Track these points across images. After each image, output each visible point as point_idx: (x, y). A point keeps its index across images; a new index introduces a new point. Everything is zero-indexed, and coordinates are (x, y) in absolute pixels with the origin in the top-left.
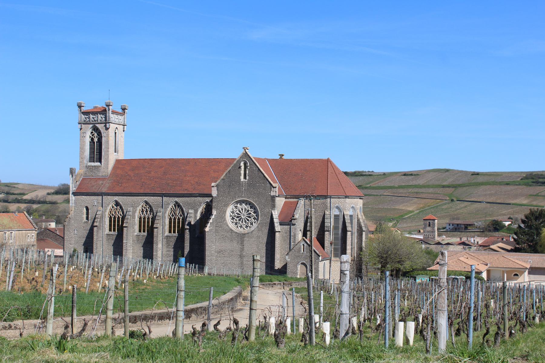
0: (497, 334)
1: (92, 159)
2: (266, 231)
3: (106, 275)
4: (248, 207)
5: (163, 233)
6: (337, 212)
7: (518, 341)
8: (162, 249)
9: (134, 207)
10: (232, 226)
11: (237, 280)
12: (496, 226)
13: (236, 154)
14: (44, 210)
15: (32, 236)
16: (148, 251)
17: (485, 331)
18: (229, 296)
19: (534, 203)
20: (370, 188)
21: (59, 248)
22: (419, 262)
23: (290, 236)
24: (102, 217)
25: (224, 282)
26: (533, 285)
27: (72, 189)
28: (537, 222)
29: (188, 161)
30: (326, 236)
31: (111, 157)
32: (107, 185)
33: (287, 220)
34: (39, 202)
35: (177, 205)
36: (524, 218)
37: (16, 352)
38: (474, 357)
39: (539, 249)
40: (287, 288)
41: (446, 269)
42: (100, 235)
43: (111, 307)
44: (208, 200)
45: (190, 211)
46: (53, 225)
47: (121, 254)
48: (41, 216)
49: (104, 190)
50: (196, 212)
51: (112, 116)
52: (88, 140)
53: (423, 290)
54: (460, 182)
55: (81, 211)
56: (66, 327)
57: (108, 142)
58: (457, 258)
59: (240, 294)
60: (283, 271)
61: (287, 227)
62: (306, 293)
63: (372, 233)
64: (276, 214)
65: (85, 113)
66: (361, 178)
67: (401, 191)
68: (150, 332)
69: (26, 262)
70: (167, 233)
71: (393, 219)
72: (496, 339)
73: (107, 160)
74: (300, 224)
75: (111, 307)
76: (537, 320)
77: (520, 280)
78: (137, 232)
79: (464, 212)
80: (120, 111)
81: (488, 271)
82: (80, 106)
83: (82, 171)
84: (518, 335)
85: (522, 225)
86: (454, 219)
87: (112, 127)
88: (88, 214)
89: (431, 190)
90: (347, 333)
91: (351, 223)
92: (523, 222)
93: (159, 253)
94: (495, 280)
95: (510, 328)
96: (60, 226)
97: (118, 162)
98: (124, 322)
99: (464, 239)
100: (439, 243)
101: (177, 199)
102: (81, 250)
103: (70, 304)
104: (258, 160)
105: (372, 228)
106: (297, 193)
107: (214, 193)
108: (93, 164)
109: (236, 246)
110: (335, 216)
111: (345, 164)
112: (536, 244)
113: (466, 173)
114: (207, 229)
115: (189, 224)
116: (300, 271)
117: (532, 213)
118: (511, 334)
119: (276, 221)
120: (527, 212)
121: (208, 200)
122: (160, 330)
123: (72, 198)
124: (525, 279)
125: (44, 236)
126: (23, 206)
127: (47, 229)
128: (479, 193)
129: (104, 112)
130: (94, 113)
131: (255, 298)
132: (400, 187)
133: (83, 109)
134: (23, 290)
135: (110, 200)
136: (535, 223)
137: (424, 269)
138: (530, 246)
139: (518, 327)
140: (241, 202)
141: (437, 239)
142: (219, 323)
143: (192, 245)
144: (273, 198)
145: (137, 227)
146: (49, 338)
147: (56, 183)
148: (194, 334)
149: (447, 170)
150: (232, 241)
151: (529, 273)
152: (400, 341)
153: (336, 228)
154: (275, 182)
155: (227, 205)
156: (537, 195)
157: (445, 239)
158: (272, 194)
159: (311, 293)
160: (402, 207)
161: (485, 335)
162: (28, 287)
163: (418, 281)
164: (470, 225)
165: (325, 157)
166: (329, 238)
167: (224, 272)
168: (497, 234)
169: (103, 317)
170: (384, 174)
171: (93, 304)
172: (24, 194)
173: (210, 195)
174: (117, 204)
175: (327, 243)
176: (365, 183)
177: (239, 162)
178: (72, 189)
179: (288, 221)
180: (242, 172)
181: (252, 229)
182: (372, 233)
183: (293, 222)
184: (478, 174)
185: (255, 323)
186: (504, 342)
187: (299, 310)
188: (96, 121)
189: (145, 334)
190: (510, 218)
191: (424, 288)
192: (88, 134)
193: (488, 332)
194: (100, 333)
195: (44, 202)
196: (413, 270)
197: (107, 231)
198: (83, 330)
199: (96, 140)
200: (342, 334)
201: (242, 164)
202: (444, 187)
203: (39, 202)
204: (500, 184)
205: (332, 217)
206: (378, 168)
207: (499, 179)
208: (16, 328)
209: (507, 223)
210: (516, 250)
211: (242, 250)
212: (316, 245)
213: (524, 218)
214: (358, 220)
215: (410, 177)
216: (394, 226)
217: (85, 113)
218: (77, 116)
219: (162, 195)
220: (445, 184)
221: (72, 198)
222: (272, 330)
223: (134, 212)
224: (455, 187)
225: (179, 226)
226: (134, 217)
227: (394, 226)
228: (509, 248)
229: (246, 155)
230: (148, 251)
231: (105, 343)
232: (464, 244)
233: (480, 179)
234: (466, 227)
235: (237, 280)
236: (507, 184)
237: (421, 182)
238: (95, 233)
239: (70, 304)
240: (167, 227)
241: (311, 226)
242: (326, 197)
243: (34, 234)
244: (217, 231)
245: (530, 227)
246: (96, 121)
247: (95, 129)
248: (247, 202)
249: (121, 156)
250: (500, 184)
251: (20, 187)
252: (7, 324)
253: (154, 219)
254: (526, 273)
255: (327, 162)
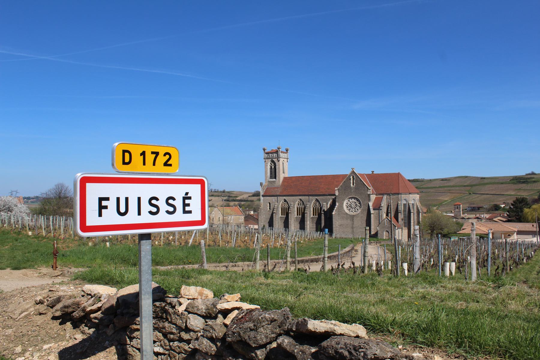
0: (503, 269)
1: (271, 177)
2: (366, 213)
3: (276, 237)
4: (355, 201)
5: (310, 216)
6: (405, 203)
7: (516, 273)
8: (309, 225)
9: (294, 202)
10: (347, 211)
11: (351, 241)
12: (496, 208)
13: (348, 172)
14: (247, 204)
15: (242, 219)
16: (302, 226)
17: (496, 268)
18: (347, 249)
19: (518, 194)
20: (423, 188)
21: (256, 225)
22: (452, 230)
23: (379, 216)
24: (278, 207)
25: (345, 242)
26: (520, 240)
27: (262, 193)
28: (521, 205)
29: (322, 177)
30: (400, 216)
31: (281, 176)
32: (280, 191)
33: (377, 207)
34: (245, 201)
35: (317, 200)
36: (512, 203)
37: (244, 279)
38: (495, 282)
39: (522, 220)
40: (378, 245)
41: (475, 232)
42: (277, 217)
43: (289, 255)
44: (333, 197)
45: (324, 204)
46: (252, 213)
47: (288, 228)
48: (246, 208)
49: (278, 194)
50: (327, 204)
51: (281, 154)
52: (269, 167)
53: (456, 244)
54: (474, 183)
55: (267, 205)
56: (265, 266)
57: (279, 168)
58: (476, 226)
59: (353, 248)
60: (376, 235)
61: (377, 211)
62: (394, 248)
63: (425, 213)
64: (371, 204)
65: (267, 153)
66: (417, 183)
67: (440, 189)
68: (309, 269)
69: (241, 232)
70: (312, 216)
71: (436, 205)
72: (502, 271)
73: (279, 177)
74: (384, 210)
75: (289, 255)
76: (525, 261)
77: (512, 238)
78: (296, 216)
79: (477, 200)
80: (285, 151)
81: (493, 233)
82: (264, 150)
83: (266, 184)
84: (514, 270)
85: (512, 207)
86: (471, 204)
87: (281, 160)
88: (270, 206)
89: (457, 188)
90: (419, 269)
91: (413, 208)
92: (512, 205)
93: (308, 227)
94: (497, 239)
95: (510, 266)
96: (256, 213)
97: (285, 178)
98: (295, 263)
99: (478, 215)
100: (463, 218)
101: (316, 197)
102: (267, 226)
103: (266, 254)
104: (360, 175)
105: (425, 211)
106: (382, 192)
107: (337, 193)
108: (272, 180)
109: (349, 222)
110: (404, 204)
111: (408, 175)
112: (521, 217)
113: (477, 178)
114: (333, 213)
115: (324, 210)
116: (385, 235)
117: (517, 200)
118: (510, 269)
119: (371, 208)
120: (515, 199)
121: (333, 197)
122: (315, 268)
123: (262, 198)
124: (515, 237)
125: (248, 219)
126: (237, 203)
127: (249, 215)
128: (486, 189)
129: (277, 152)
130: (271, 153)
131: (367, 251)
132: (440, 187)
133: (266, 151)
134: (240, 247)
135: (281, 199)
136: (519, 205)
137: (455, 233)
138: (517, 219)
139: (514, 265)
140: (351, 198)
141: (462, 215)
142: (344, 264)
143: (325, 221)
144: (369, 195)
145: (296, 213)
146: (259, 272)
147: (253, 190)
148: (332, 270)
149: (467, 177)
150: (347, 219)
151: (517, 234)
152: (447, 273)
153: (404, 211)
154: (370, 187)
155: (344, 200)
156: (520, 189)
157: (466, 216)
158: (369, 193)
159: (393, 247)
160: (440, 198)
161: (497, 269)
162: (242, 245)
163: (452, 239)
164: (481, 207)
165: (397, 172)
166: (401, 216)
167: (343, 236)
168: (497, 212)
169: (285, 260)
170: (430, 180)
171: (278, 254)
172: (237, 197)
173: (334, 195)
174: (285, 201)
175: (400, 220)
176: (420, 185)
177: (350, 176)
178: (262, 193)
179: (378, 207)
180: (352, 182)
181: (358, 212)
182: (425, 213)
183: (381, 208)
184: (484, 178)
185: (367, 264)
186: (507, 273)
187: (389, 256)
188: (273, 157)
189: (306, 270)
190: (504, 203)
191: (456, 243)
192: (269, 164)
193: (498, 268)
194: (282, 269)
195: (247, 201)
196: (449, 233)
197: (280, 215)
198: (274, 267)
199: (273, 167)
200: (416, 269)
201: (351, 177)
202: (465, 186)
203: (245, 201)
204: (498, 183)
205: (402, 205)
206: (427, 177)
207: (497, 181)
208: (238, 266)
209: (502, 206)
210: (508, 221)
211: (353, 224)
212: (394, 221)
213: (512, 203)
214: (417, 206)
215: (445, 181)
216: (437, 209)
217: (267, 153)
218: (262, 155)
219: (309, 195)
220: (465, 184)
221: (262, 198)
222: (374, 268)
223: (294, 205)
224: (472, 186)
225: (318, 212)
226: (294, 208)
227: (437, 209)
228: (504, 220)
229: (353, 172)
230: (302, 226)
231: (288, 275)
232: (477, 218)
233: (486, 181)
234: (479, 208)
235: (351, 241)
236: (502, 183)
237: (451, 184)
238: (274, 217)
239: (266, 254)
240: (312, 212)
241: (391, 210)
242: (398, 194)
243: (243, 217)
244: (339, 214)
245: (516, 208)
246: (273, 157)
247: (273, 161)
248: (355, 198)
249: (287, 175)
250: (498, 183)
251: (235, 193)
252: (234, 264)
253: (305, 208)
254: (515, 234)
255: (399, 174)
